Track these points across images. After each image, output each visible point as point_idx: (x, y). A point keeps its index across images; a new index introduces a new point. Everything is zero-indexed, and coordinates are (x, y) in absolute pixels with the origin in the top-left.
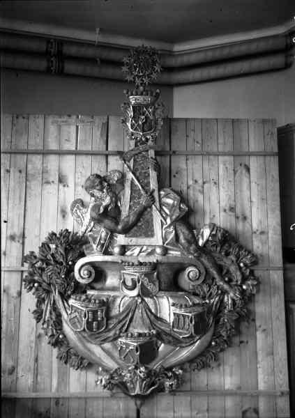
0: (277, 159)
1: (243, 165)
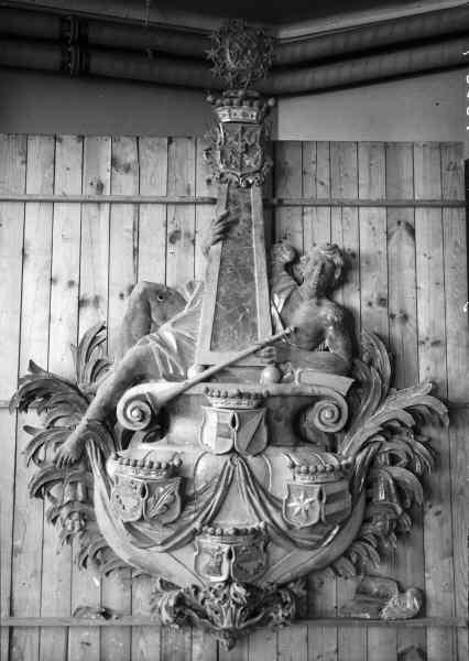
0: (463, 213)
1: (402, 224)
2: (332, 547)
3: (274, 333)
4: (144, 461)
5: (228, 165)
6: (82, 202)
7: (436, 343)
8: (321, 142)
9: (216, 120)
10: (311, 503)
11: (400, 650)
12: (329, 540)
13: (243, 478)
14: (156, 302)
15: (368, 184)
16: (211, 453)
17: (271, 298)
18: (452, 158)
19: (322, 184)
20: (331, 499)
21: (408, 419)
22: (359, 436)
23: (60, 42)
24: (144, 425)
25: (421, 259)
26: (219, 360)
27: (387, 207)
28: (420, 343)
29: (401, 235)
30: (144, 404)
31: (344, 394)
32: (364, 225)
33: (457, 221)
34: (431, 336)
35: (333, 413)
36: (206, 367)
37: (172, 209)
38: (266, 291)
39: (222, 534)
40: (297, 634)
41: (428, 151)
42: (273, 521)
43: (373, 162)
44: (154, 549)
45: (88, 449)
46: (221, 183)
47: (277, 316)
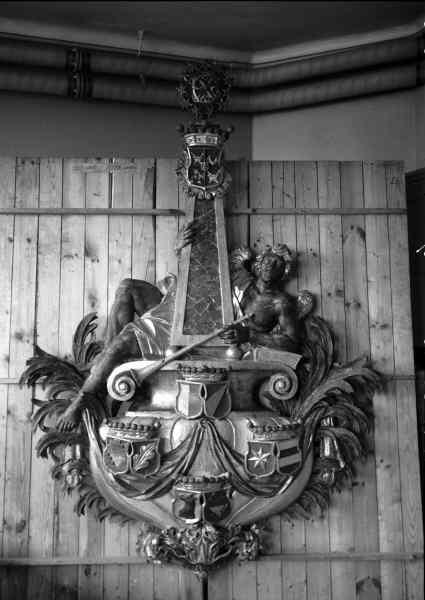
0: (405, 218)
2: (289, 489)
3: (235, 319)
4: (130, 425)
5: (195, 182)
6: (15, 214)
7: (384, 326)
8: (287, 162)
9: (185, 145)
10: (269, 456)
11: (358, 580)
12: (284, 488)
13: (211, 437)
14: (139, 296)
15: (325, 194)
16: (184, 419)
17: (232, 289)
18: (396, 175)
19: (288, 196)
20: (285, 453)
21: (349, 389)
22: (308, 405)
23: (66, 70)
24: (129, 396)
25: (370, 256)
26: (191, 342)
27: (342, 215)
28: (371, 326)
29: (354, 238)
30: (130, 379)
31: (294, 367)
32: (323, 230)
33: (400, 226)
34: (381, 321)
35: (285, 383)
36: (180, 348)
37: (17, 218)
38: (228, 285)
39: (194, 482)
40: (270, 567)
41: (375, 168)
42: (236, 472)
43: (330, 178)
44: (139, 498)
45: (84, 416)
46: (190, 196)
47: (238, 305)
